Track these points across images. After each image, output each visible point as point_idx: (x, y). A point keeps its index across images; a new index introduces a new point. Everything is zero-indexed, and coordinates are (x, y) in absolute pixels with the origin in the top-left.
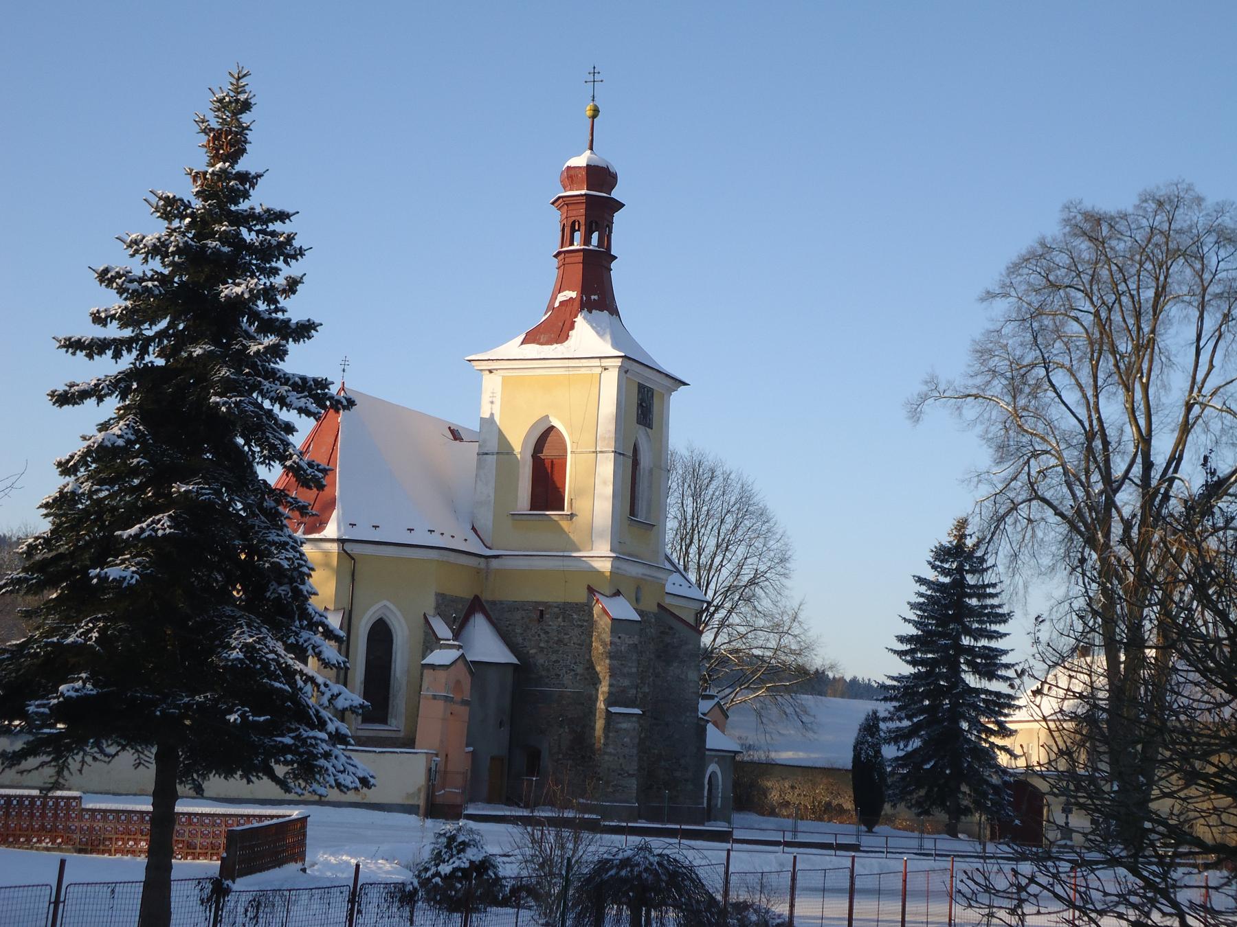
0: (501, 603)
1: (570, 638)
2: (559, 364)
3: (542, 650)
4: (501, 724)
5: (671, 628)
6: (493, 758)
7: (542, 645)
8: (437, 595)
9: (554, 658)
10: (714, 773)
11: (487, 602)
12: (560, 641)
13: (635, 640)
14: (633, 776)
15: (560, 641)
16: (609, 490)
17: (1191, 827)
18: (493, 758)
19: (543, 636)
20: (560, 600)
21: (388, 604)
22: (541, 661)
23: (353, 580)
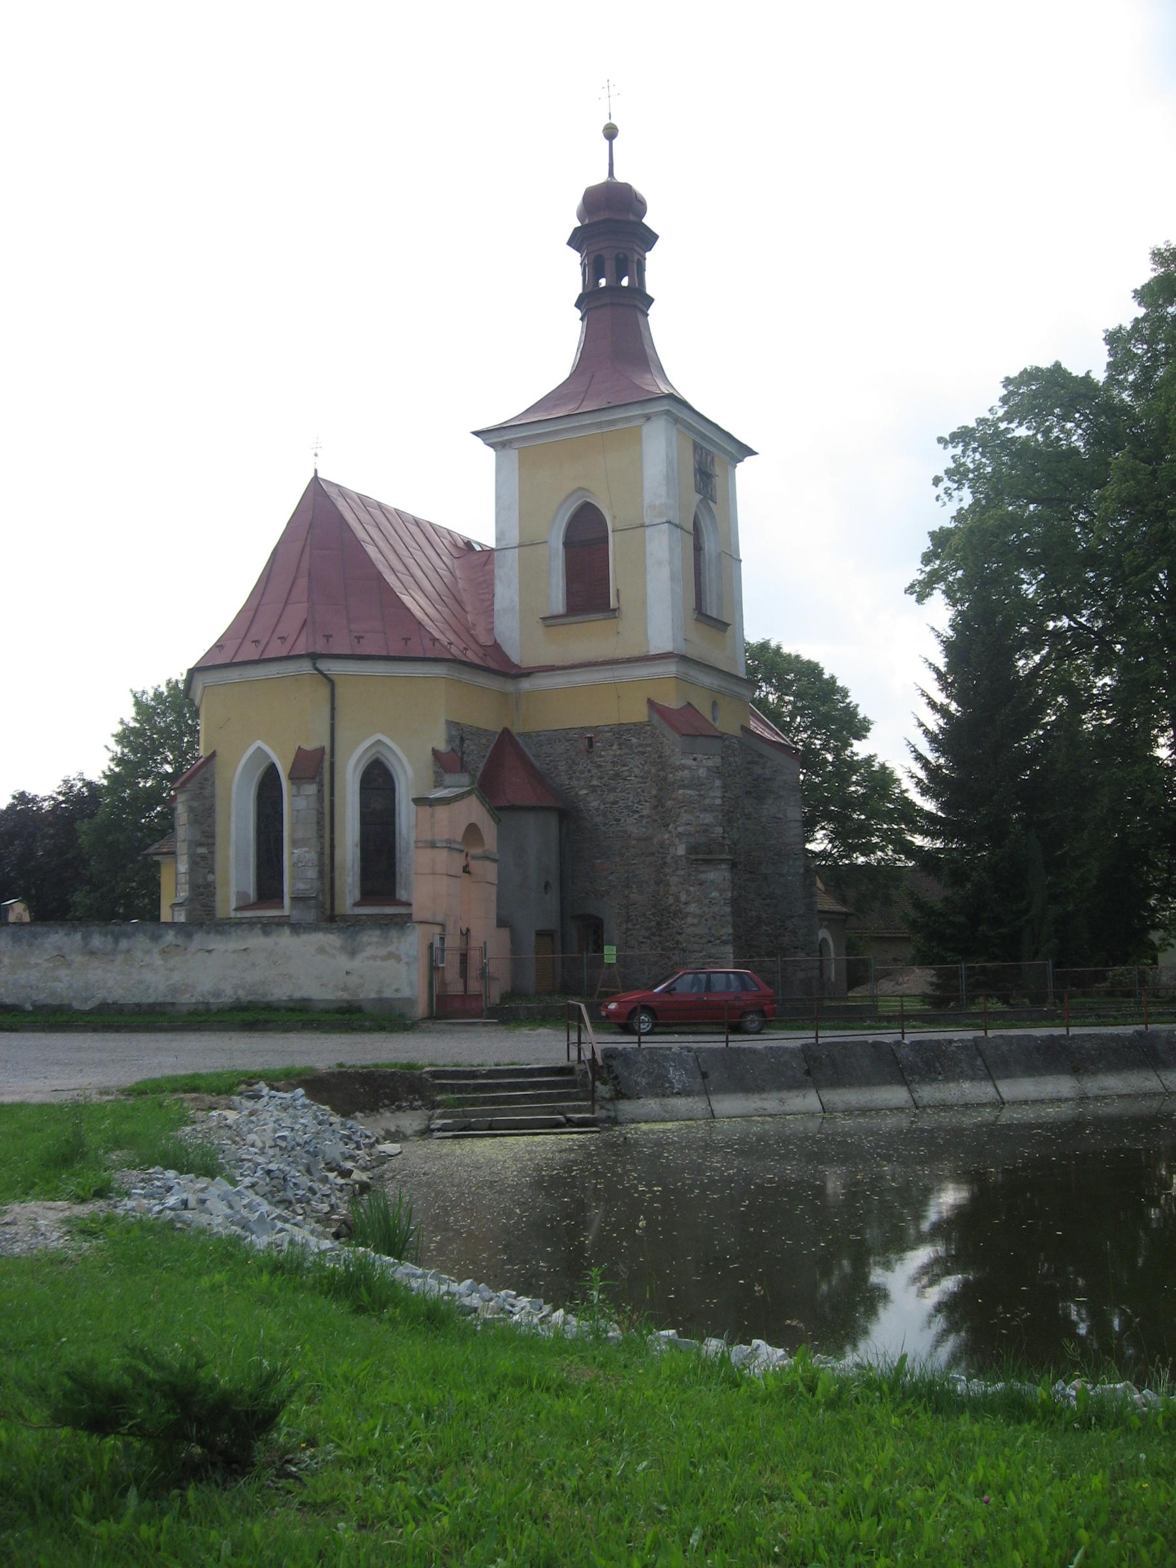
0: (538, 734)
1: (630, 771)
2: (587, 420)
3: (594, 789)
4: (547, 886)
5: (761, 756)
6: (540, 934)
7: (595, 782)
8: (449, 723)
9: (611, 797)
10: (824, 940)
11: (520, 735)
12: (617, 775)
13: (717, 761)
14: (725, 943)
15: (617, 775)
16: (665, 572)
17: (383, 1186)
18: (540, 934)
19: (594, 771)
20: (613, 720)
21: (582, 1006)
22: (595, 804)
23: (333, 709)
